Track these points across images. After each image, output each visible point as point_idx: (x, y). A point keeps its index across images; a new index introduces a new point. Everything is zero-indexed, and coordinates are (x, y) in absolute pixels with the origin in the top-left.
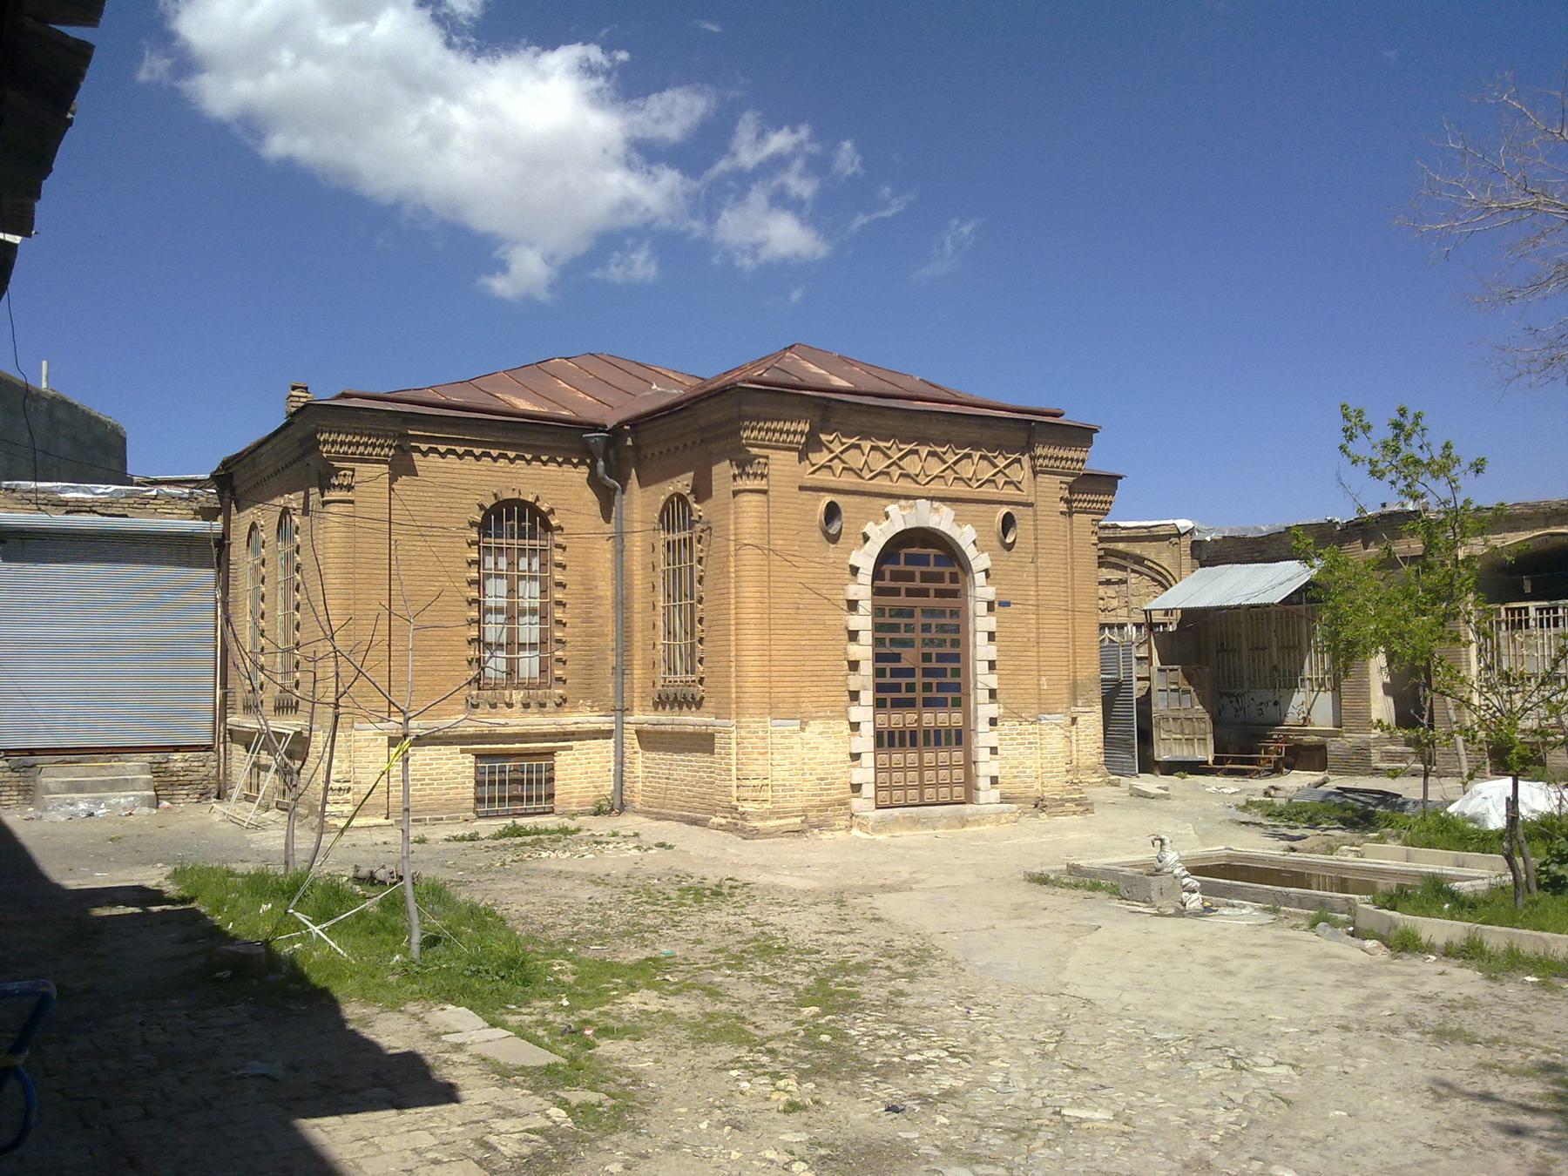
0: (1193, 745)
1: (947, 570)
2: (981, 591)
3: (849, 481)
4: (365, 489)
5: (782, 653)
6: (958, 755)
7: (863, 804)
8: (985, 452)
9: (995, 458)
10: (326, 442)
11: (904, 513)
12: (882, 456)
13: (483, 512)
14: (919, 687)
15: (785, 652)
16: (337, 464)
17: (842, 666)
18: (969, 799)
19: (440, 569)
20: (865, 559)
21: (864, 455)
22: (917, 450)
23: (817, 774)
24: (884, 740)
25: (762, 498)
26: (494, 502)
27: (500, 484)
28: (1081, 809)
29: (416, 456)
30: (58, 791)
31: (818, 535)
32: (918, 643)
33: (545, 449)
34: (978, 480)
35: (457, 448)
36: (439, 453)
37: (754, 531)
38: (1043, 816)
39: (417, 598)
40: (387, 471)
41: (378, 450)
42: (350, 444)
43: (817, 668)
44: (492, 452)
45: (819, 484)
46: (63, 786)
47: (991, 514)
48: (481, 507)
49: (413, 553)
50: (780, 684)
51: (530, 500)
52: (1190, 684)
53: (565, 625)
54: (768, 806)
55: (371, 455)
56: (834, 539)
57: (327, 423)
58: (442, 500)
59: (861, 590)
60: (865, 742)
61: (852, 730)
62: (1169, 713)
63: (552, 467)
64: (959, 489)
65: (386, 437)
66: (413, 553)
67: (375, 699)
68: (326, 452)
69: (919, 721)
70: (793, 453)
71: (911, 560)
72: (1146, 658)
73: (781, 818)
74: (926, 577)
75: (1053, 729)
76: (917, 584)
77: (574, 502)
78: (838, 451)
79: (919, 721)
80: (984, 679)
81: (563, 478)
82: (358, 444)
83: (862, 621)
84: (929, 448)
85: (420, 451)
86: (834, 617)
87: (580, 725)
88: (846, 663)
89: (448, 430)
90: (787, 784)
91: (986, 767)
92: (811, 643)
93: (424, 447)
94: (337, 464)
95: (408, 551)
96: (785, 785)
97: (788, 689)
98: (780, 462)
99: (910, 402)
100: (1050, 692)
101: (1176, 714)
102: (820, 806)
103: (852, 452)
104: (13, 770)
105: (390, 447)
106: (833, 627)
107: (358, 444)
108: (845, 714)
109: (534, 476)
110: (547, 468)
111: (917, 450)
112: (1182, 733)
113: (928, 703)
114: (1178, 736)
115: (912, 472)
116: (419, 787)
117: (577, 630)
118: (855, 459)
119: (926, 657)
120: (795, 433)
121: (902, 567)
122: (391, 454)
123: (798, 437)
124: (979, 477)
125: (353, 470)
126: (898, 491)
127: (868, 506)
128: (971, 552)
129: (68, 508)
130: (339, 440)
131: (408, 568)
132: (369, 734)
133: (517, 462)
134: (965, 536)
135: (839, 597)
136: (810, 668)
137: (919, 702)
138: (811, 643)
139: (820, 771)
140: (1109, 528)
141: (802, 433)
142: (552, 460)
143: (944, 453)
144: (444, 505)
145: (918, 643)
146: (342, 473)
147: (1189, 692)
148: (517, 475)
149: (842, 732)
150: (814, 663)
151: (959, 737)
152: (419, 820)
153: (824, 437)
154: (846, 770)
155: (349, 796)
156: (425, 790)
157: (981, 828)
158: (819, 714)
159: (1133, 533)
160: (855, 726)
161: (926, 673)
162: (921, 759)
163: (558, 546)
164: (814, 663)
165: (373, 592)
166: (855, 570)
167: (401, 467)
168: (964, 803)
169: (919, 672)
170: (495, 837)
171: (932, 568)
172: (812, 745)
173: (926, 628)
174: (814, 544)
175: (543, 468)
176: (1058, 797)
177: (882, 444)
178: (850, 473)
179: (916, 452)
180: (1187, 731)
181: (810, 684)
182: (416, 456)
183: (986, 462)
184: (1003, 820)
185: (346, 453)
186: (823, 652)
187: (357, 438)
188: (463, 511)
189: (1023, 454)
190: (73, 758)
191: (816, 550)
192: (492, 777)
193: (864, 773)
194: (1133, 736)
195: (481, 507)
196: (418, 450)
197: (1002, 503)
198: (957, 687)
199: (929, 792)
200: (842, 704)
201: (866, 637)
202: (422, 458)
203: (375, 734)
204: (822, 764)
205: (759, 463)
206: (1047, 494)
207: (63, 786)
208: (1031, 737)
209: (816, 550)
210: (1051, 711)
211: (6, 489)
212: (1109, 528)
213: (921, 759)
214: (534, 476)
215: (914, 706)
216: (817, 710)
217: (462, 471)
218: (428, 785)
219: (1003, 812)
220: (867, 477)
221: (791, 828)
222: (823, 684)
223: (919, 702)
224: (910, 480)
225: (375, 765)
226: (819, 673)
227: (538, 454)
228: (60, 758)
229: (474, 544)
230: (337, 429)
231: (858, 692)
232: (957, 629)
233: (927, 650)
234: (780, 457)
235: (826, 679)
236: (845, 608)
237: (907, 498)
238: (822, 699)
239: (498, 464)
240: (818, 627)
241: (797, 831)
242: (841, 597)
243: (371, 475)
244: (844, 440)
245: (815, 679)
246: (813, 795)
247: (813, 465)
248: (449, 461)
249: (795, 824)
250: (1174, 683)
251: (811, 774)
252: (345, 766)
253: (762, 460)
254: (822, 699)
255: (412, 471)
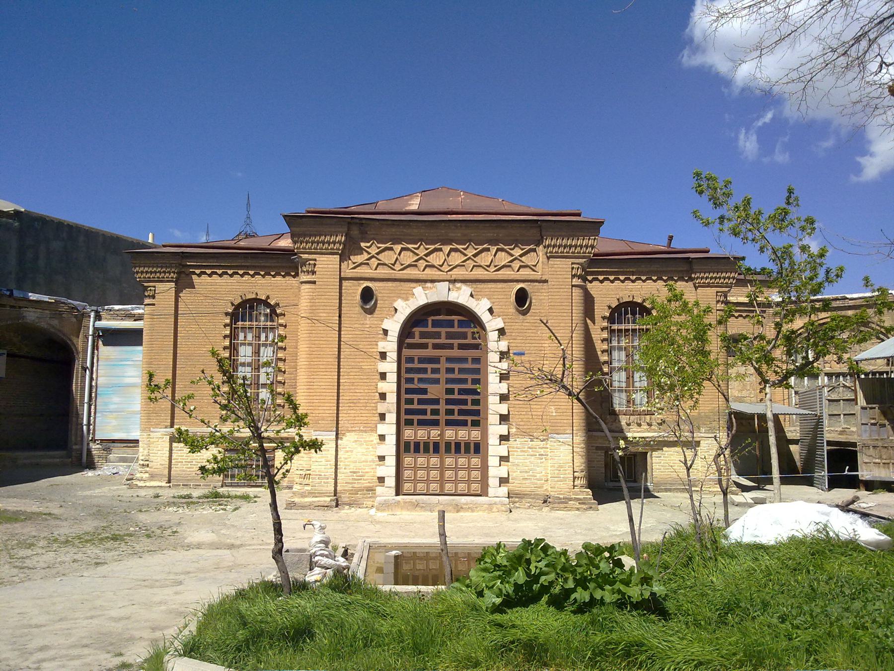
0: (889, 468)
1: (469, 331)
2: (495, 344)
3: (383, 272)
4: (161, 297)
5: (322, 387)
6: (476, 461)
7: (387, 492)
8: (501, 246)
9: (465, 249)
10: (137, 272)
11: (426, 292)
12: (411, 254)
13: (234, 307)
14: (443, 412)
15: (324, 387)
16: (146, 284)
17: (375, 396)
18: (484, 492)
19: (206, 340)
20: (394, 326)
21: (396, 254)
22: (441, 248)
23: (350, 469)
24: (403, 448)
25: (312, 286)
26: (241, 300)
27: (245, 290)
28: (585, 507)
29: (194, 277)
30: (115, 461)
31: (358, 309)
32: (442, 381)
33: (665, 273)
34: (495, 266)
35: (218, 271)
36: (218, 274)
37: (306, 308)
38: (546, 509)
39: (192, 358)
40: (174, 286)
41: (167, 275)
42: (151, 273)
43: (354, 398)
44: (239, 271)
45: (359, 275)
46: (117, 459)
47: (508, 290)
48: (609, 307)
49: (190, 332)
50: (320, 408)
51: (639, 301)
52: (885, 419)
53: (284, 372)
54: (309, 488)
55: (164, 278)
56: (371, 312)
57: (138, 262)
58: (208, 301)
59: (390, 346)
60: (389, 448)
61: (380, 440)
62: (869, 442)
63: (279, 278)
64: (479, 273)
65: (171, 267)
66: (190, 332)
67: (163, 415)
68: (139, 278)
69: (441, 435)
70: (335, 256)
71: (436, 324)
72: (853, 400)
73: (316, 497)
74: (449, 336)
75: (560, 445)
76: (443, 340)
77: (292, 299)
78: (470, 255)
79: (441, 435)
80: (495, 407)
81: (286, 284)
82: (156, 272)
83: (390, 366)
84: (402, 246)
85: (196, 274)
86: (369, 364)
87: (290, 434)
88: (377, 394)
89: (211, 260)
90: (323, 474)
91: (496, 471)
92: (349, 381)
93: (198, 271)
94: (146, 284)
95: (187, 331)
96: (320, 475)
97: (327, 411)
98: (325, 263)
99: (446, 216)
100: (558, 417)
101: (875, 443)
102: (352, 490)
103: (386, 253)
104: (104, 450)
105: (174, 273)
106: (368, 370)
107: (156, 272)
108: (375, 429)
109: (266, 284)
110: (275, 279)
111: (441, 248)
112: (880, 458)
113: (449, 423)
114: (877, 461)
115: (437, 263)
116: (189, 466)
117: (293, 375)
118: (388, 257)
119: (450, 391)
120: (334, 243)
121: (430, 329)
122: (175, 277)
123: (337, 245)
124: (496, 264)
125: (155, 287)
126: (424, 277)
127: (400, 288)
128: (485, 317)
129: (135, 318)
130: (145, 271)
131: (187, 340)
132: (159, 435)
133: (256, 276)
134: (480, 308)
135: (373, 350)
136: (348, 398)
137: (442, 422)
138: (349, 381)
139: (352, 467)
140: (839, 299)
141: (340, 243)
142: (660, 278)
143: (465, 249)
144: (210, 304)
145: (442, 381)
146: (149, 289)
147: (884, 426)
148: (255, 284)
149: (372, 441)
150: (351, 394)
151: (478, 448)
152: (187, 485)
153: (363, 244)
154: (374, 467)
155: (148, 469)
156: (193, 468)
157: (475, 514)
158: (354, 429)
159: (858, 302)
160: (382, 438)
161: (448, 402)
162: (442, 462)
163: (281, 325)
164: (351, 394)
165: (164, 354)
166: (386, 332)
167: (183, 282)
168: (481, 496)
169: (442, 402)
170: (199, 498)
171: (456, 329)
172: (348, 449)
173: (450, 370)
174: (354, 316)
175: (273, 279)
176: (562, 496)
177: (410, 246)
178: (385, 266)
179: (391, 249)
180: (884, 457)
181: (347, 408)
182: (194, 277)
183: (503, 253)
184: (494, 510)
185: (149, 278)
186: (359, 387)
187: (155, 269)
188: (221, 307)
189: (538, 245)
190: (132, 445)
191: (356, 319)
192: (258, 463)
193: (388, 470)
194: (824, 458)
195: (609, 307)
196: (194, 273)
197: (518, 281)
198: (477, 413)
199: (448, 487)
200: (373, 422)
201: (392, 377)
202: (198, 278)
203: (162, 435)
204: (355, 462)
205: (309, 264)
206: (558, 273)
207: (117, 459)
208: (542, 450)
209: (356, 319)
210: (561, 432)
211: (107, 310)
212: (839, 299)
213: (442, 462)
214: (266, 284)
215: (439, 425)
216: (352, 425)
217: (221, 284)
218: (194, 465)
219: (495, 504)
220: (398, 269)
221: (322, 504)
222: (357, 408)
223: (442, 422)
224: (435, 269)
225: (162, 452)
226: (355, 401)
227: (268, 271)
228: (125, 445)
229: (228, 326)
230: (699, 271)
231: (385, 414)
232: (477, 371)
233: (450, 386)
234: (325, 259)
235: (361, 405)
236: (378, 357)
237: (433, 281)
238: (357, 418)
239: (244, 279)
240: (355, 370)
241: (327, 506)
242: (375, 350)
243: (165, 289)
244: (379, 245)
245: (352, 405)
246: (346, 483)
247: (402, 265)
248: (203, 278)
249: (325, 501)
250: (874, 419)
251: (345, 468)
252: (146, 452)
253: (311, 262)
254: (357, 418)
255: (192, 286)
